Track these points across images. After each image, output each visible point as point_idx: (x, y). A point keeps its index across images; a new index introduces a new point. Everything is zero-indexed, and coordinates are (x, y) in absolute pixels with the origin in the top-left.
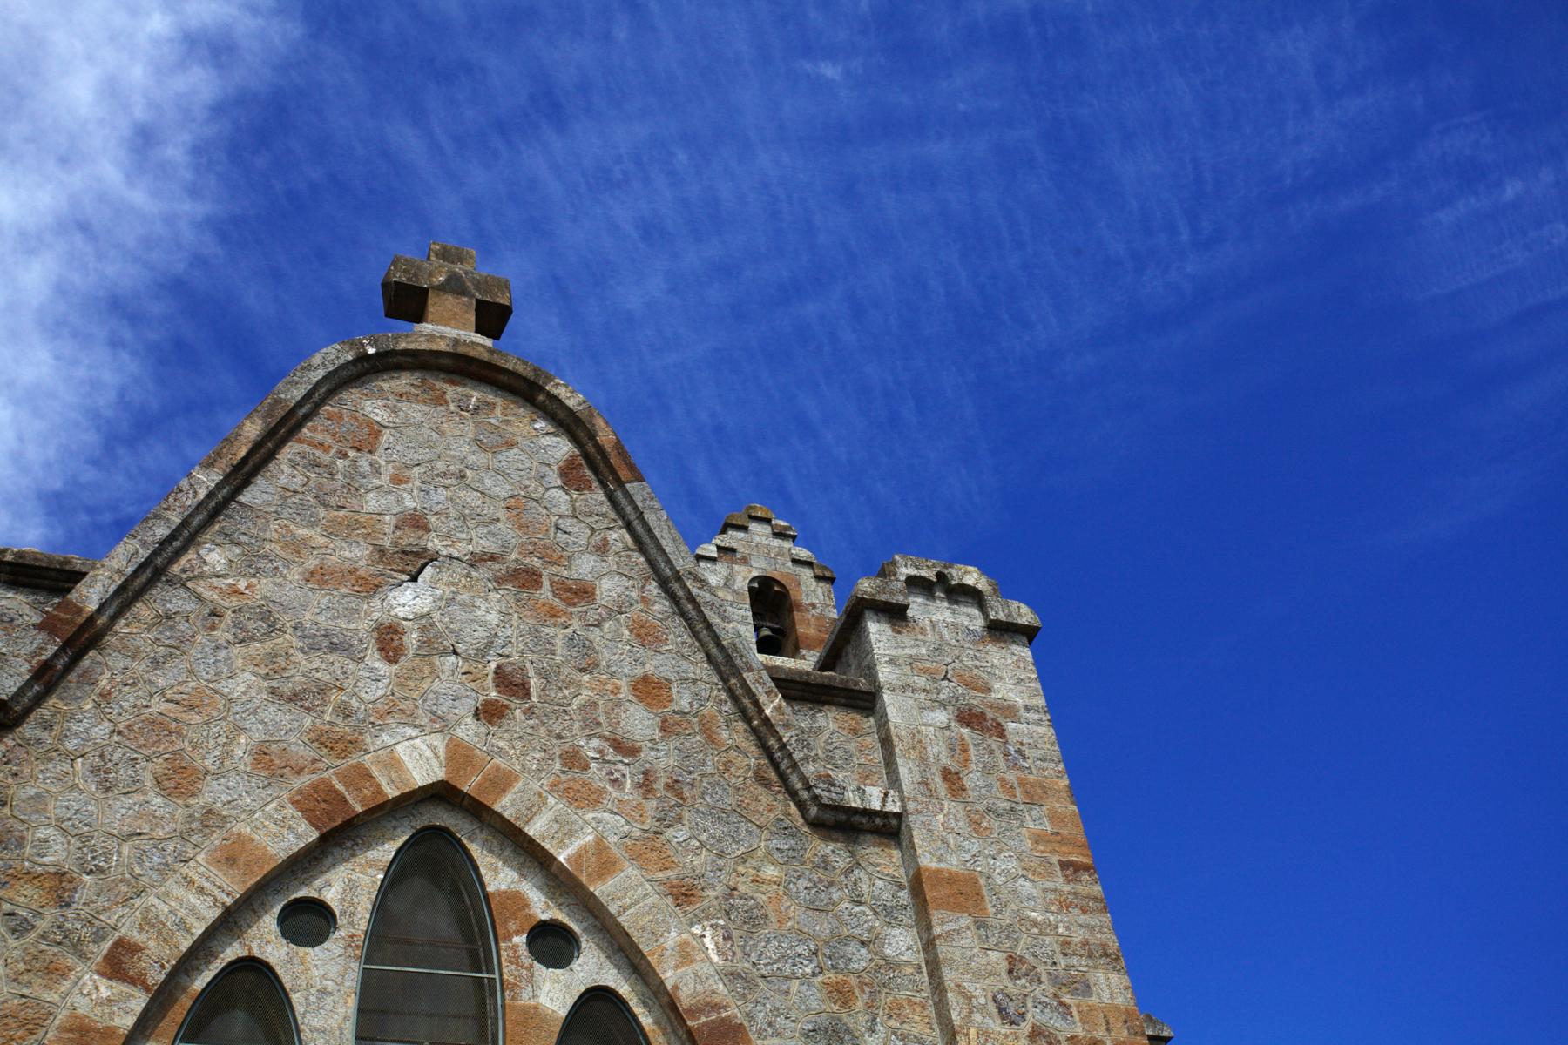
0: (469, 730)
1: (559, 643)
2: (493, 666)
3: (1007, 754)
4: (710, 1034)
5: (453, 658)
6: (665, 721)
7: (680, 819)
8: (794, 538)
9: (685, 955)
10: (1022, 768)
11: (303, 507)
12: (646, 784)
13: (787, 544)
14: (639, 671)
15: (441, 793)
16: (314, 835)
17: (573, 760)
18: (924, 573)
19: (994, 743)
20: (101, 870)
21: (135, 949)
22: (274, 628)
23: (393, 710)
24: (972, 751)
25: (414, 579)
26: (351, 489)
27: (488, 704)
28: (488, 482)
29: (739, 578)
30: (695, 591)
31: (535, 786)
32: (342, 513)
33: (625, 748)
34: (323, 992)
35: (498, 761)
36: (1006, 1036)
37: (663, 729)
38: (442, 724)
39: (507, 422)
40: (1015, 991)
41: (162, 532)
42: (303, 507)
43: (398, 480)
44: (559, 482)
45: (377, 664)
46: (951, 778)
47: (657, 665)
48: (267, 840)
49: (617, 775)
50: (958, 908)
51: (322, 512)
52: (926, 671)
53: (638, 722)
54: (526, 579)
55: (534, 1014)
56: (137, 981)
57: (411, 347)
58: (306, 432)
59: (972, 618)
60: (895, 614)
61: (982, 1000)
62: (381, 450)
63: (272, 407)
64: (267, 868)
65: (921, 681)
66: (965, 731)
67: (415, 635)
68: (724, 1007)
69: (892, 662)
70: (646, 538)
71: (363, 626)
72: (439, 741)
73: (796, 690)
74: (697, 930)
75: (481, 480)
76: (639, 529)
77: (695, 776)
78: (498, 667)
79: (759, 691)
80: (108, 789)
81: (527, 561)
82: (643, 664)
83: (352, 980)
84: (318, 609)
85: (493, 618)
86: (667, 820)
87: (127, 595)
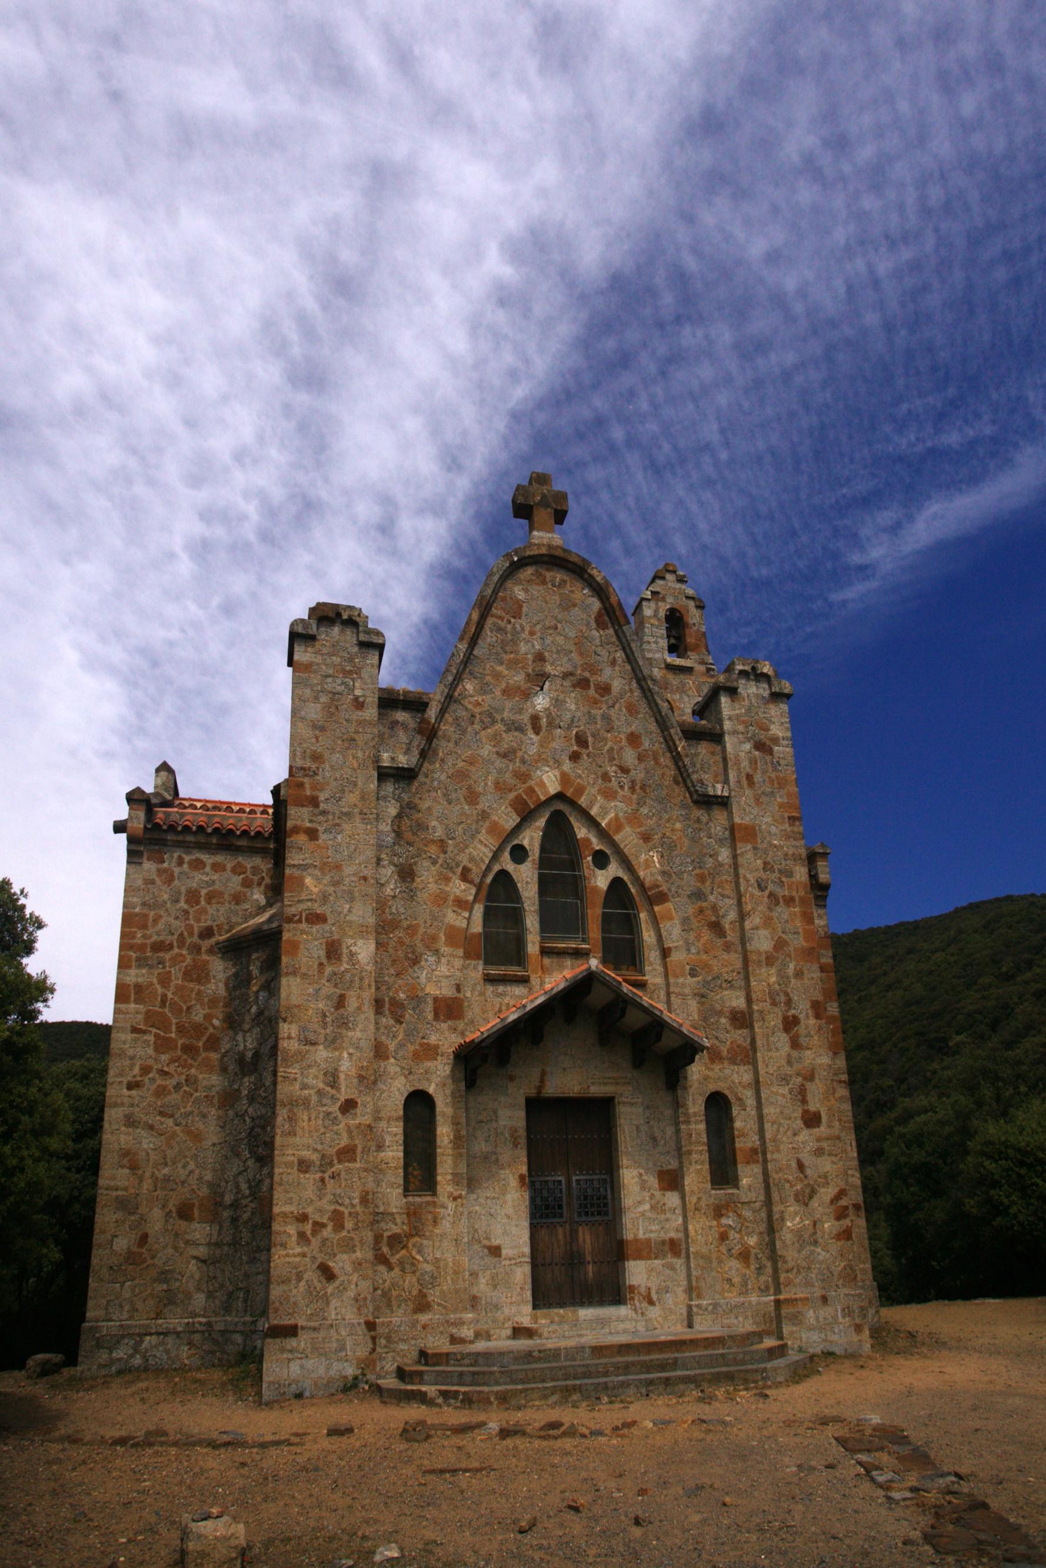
0: (567, 766)
1: (599, 718)
3: (773, 764)
12: (632, 789)
14: (629, 731)
15: (560, 796)
16: (518, 820)
17: (606, 777)
19: (768, 758)
22: (494, 722)
25: (542, 689)
32: (512, 656)
33: (625, 770)
34: (527, 883)
35: (579, 780)
38: (558, 763)
39: (572, 592)
43: (532, 633)
45: (532, 736)
46: (749, 777)
47: (635, 726)
50: (747, 841)
52: (743, 722)
53: (629, 756)
54: (583, 684)
55: (596, 889)
56: (471, 882)
62: (523, 617)
65: (741, 728)
71: (525, 718)
72: (557, 773)
79: (676, 738)
84: (508, 709)
85: (573, 707)
86: (641, 803)
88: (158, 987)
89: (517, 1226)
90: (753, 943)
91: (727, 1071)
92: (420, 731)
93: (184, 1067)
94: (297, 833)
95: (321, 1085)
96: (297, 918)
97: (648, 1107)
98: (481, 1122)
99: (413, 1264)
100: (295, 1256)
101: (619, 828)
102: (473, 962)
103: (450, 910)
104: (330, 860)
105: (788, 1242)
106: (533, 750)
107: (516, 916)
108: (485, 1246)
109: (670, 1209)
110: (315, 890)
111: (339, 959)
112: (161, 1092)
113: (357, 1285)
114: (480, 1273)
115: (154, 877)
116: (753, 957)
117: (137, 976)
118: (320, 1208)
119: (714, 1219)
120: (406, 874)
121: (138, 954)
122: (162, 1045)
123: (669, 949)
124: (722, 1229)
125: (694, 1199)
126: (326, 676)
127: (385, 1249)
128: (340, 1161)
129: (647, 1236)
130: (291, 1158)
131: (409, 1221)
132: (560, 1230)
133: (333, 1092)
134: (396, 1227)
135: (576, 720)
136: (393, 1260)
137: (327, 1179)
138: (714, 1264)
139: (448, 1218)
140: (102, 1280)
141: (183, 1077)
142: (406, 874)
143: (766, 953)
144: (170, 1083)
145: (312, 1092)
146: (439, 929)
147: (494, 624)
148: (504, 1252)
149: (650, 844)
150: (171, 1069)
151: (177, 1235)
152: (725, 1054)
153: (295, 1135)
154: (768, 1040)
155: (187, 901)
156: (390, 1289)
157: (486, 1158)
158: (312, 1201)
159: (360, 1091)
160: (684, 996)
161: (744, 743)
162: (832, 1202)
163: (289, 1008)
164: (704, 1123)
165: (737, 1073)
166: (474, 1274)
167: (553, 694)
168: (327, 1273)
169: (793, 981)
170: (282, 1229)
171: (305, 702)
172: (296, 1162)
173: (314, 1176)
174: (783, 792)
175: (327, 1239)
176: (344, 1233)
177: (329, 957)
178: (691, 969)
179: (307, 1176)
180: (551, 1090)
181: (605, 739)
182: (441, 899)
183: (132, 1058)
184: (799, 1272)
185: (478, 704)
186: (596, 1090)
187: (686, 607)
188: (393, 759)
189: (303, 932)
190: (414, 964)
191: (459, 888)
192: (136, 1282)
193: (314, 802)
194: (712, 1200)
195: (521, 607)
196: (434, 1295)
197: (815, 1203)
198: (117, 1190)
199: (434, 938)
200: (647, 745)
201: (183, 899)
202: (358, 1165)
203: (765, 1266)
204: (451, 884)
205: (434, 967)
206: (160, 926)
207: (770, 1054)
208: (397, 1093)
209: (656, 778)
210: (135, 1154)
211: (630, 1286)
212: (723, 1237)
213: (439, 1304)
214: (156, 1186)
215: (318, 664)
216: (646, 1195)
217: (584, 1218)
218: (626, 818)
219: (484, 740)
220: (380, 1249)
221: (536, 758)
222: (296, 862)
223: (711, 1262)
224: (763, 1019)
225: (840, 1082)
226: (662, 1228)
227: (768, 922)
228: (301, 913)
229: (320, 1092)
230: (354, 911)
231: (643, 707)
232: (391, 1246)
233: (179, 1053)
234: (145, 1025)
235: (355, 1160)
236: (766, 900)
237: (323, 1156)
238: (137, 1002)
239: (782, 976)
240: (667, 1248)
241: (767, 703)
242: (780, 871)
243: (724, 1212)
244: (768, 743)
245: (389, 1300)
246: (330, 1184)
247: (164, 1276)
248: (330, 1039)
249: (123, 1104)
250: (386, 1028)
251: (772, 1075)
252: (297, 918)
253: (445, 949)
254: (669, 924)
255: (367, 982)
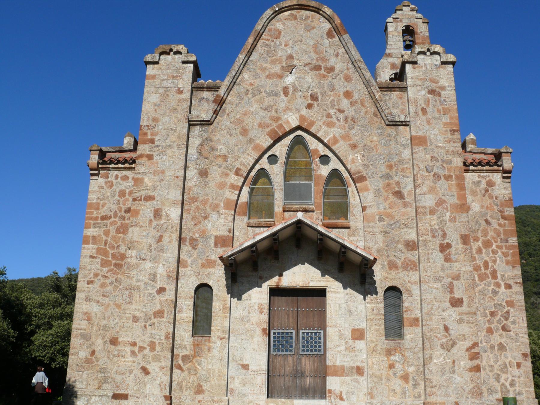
1: (326, 85)
2: (310, 94)
3: (440, 101)
6: (351, 102)
7: (354, 128)
9: (353, 161)
10: (444, 105)
11: (264, 58)
12: (346, 120)
14: (345, 90)
15: (299, 128)
16: (272, 142)
17: (329, 116)
19: (437, 98)
22: (260, 92)
23: (287, 109)
25: (291, 73)
28: (308, 41)
29: (399, 27)
30: (360, 65)
32: (274, 58)
33: (341, 111)
34: (277, 174)
38: (298, 110)
39: (313, 21)
41: (234, 73)
42: (264, 58)
43: (286, 45)
46: (424, 111)
48: (263, 144)
51: (269, 59)
52: (421, 79)
53: (345, 103)
54: (318, 68)
55: (320, 176)
56: (241, 176)
58: (263, 36)
62: (281, 37)
65: (419, 83)
66: (430, 96)
70: (348, 50)
71: (280, 89)
72: (298, 116)
73: (384, 88)
74: (356, 155)
75: (306, 41)
76: (346, 48)
79: (375, 91)
83: (282, 171)
84: (269, 85)
85: (310, 80)
86: (351, 128)
87: (229, 90)
88: (103, 236)
89: (259, 354)
91: (401, 275)
92: (215, 101)
93: (114, 274)
94: (142, 157)
95: (147, 280)
96: (138, 199)
99: (195, 370)
101: (336, 141)
102: (241, 217)
103: (227, 190)
105: (434, 371)
106: (283, 105)
111: (160, 217)
112: (103, 285)
113: (161, 378)
115: (104, 185)
116: (420, 210)
117: (93, 232)
118: (144, 340)
122: (104, 264)
126: (163, 80)
129: (341, 364)
130: (129, 315)
132: (290, 358)
133: (153, 283)
135: (311, 87)
136: (184, 368)
137: (148, 326)
138: (384, 381)
139: (217, 349)
140: (73, 370)
141: (114, 279)
144: (108, 281)
145: (142, 283)
146: (221, 200)
147: (263, 43)
148: (250, 368)
149: (355, 150)
150: (109, 275)
151: (109, 352)
152: (400, 265)
153: (132, 304)
154: (428, 257)
155: (119, 196)
157: (243, 319)
158: (139, 336)
159: (168, 283)
161: (421, 90)
162: (467, 350)
164: (383, 303)
165: (408, 276)
168: (146, 371)
169: (448, 223)
174: (447, 116)
176: (156, 352)
177: (155, 217)
178: (379, 218)
179: (137, 324)
181: (329, 96)
182: (222, 186)
183: (90, 270)
184: (440, 388)
185: (251, 84)
187: (416, 24)
189: (142, 205)
190: (205, 219)
192: (90, 371)
193: (152, 141)
196: (206, 386)
197: (455, 350)
198: (81, 330)
200: (357, 97)
201: (117, 195)
202: (164, 320)
203: (419, 384)
204: (229, 177)
206: (105, 208)
207: (429, 265)
209: (362, 114)
210: (90, 314)
211: (329, 390)
212: (391, 366)
213: (209, 391)
214: (99, 329)
215: (159, 75)
216: (343, 342)
222: (140, 171)
223: (381, 380)
224: (425, 245)
225: (516, 283)
227: (432, 190)
229: (146, 283)
232: (183, 361)
233: (112, 267)
234: (96, 254)
235: (163, 317)
236: (432, 177)
237: (146, 315)
238: (93, 244)
239: (441, 221)
240: (355, 371)
241: (439, 67)
242: (443, 161)
243: (393, 352)
247: (103, 370)
248: (153, 257)
249: (85, 291)
252: (138, 199)
253: (222, 211)
254: (366, 193)
255: (175, 228)
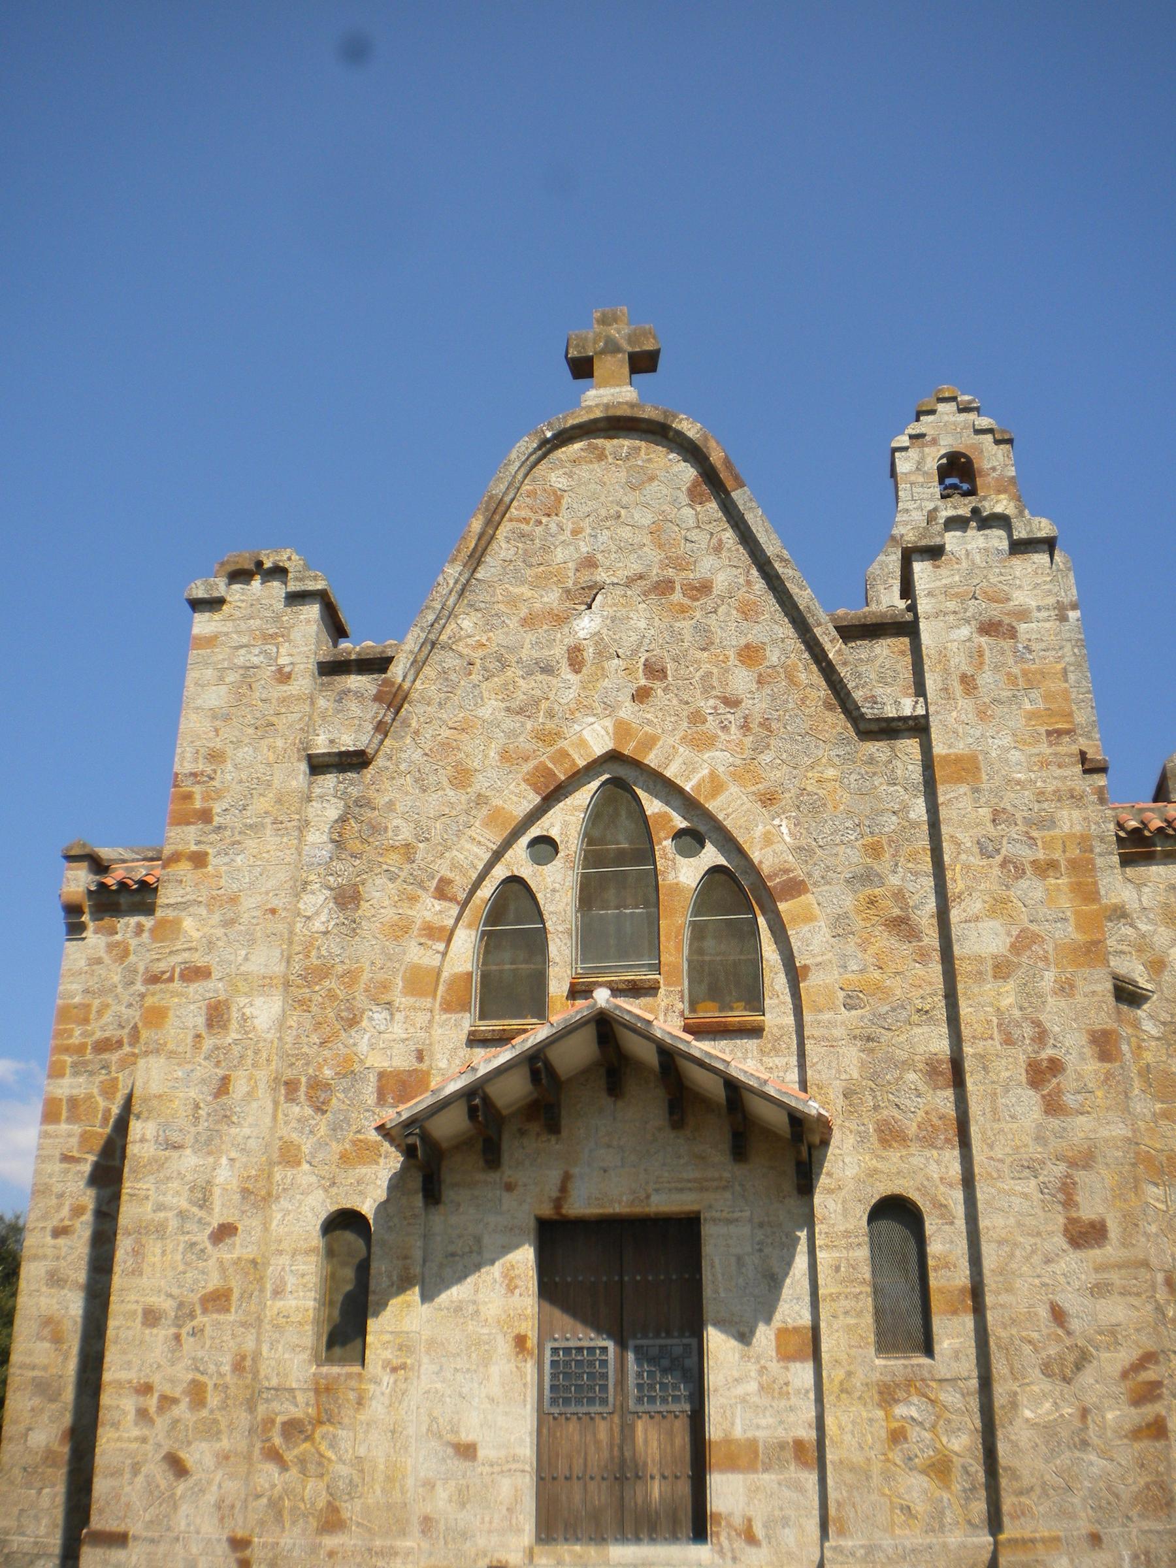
0: (628, 711)
2: (643, 660)
4: (782, 889)
5: (616, 661)
7: (768, 746)
8: (977, 409)
12: (745, 727)
13: (972, 416)
14: (743, 642)
15: (614, 757)
16: (538, 799)
17: (697, 718)
18: (960, 512)
19: (1007, 644)
20: (427, 839)
21: (449, 882)
22: (504, 666)
23: (582, 707)
24: (987, 653)
25: (590, 607)
26: (545, 549)
27: (639, 689)
28: (637, 516)
29: (929, 459)
31: (671, 741)
32: (542, 568)
33: (732, 702)
34: (554, 890)
35: (647, 728)
36: (983, 867)
37: (759, 682)
38: (610, 708)
39: (649, 460)
40: (995, 834)
41: (431, 617)
43: (575, 532)
44: (687, 501)
45: (569, 677)
46: (967, 681)
47: (756, 633)
49: (726, 722)
50: (960, 780)
51: (529, 572)
52: (957, 595)
53: (741, 680)
55: (676, 888)
56: (452, 899)
57: (576, 421)
59: (997, 539)
60: (935, 553)
61: (969, 844)
63: (488, 503)
64: (513, 824)
65: (951, 605)
67: (591, 650)
68: (792, 871)
69: (930, 594)
71: (558, 652)
72: (609, 723)
74: (777, 822)
77: (781, 712)
78: (646, 660)
80: (425, 791)
81: (665, 573)
82: (746, 635)
84: (529, 646)
85: (642, 624)
86: (760, 747)
88: (99, 1099)
89: (506, 1414)
90: (967, 944)
95: (184, 1205)
97: (761, 1225)
98: (453, 1255)
99: (320, 1464)
100: (130, 1440)
102: (454, 1016)
103: (413, 943)
104: (222, 891)
105: (1024, 1443)
107: (537, 943)
108: (449, 1444)
109: (798, 1391)
110: (196, 935)
111: (225, 1027)
114: (439, 1483)
117: (71, 1087)
118: (173, 1376)
119: (879, 1405)
120: (347, 898)
121: (75, 1058)
123: (806, 967)
124: (895, 1425)
125: (840, 1374)
127: (277, 1440)
128: (205, 1311)
129: (750, 1435)
130: (134, 1307)
131: (317, 1401)
134: (300, 1407)
136: (289, 1456)
137: (184, 1336)
138: (876, 1480)
142: (347, 898)
143: (994, 957)
145: (170, 1214)
146: (395, 971)
148: (481, 1453)
152: (912, 1129)
153: (141, 1274)
154: (993, 1101)
156: (281, 1498)
158: (159, 1366)
159: (243, 1212)
160: (831, 1043)
162: (1125, 1375)
163: (145, 1100)
165: (938, 1162)
166: (430, 1485)
167: (610, 611)
170: (114, 1403)
171: (203, 686)
172: (140, 1311)
173: (163, 1333)
174: (1035, 694)
175: (178, 1421)
176: (204, 1413)
177: (210, 1025)
179: (155, 1331)
180: (580, 1205)
182: (401, 929)
183: (61, 1196)
186: (663, 1203)
188: (332, 742)
189: (175, 994)
190: (351, 1026)
191: (431, 909)
193: (205, 816)
194: (876, 1376)
195: (559, 499)
196: (350, 1510)
197: (1087, 1377)
199: (385, 986)
202: (231, 1317)
205: (382, 1028)
206: (107, 1018)
208: (310, 1215)
213: (358, 1524)
215: (227, 634)
216: (753, 1368)
217: (646, 1407)
218: (733, 774)
219: (486, 694)
220: (269, 1440)
221: (573, 706)
222: (172, 901)
224: (985, 1068)
226: (781, 1422)
228: (173, 969)
229: (182, 1215)
230: (252, 958)
231: (771, 604)
236: (996, 871)
237: (181, 1305)
238: (69, 1120)
239: (1030, 995)
240: (789, 1454)
244: (1007, 620)
245: (280, 1513)
246: (188, 1343)
249: (45, 1257)
250: (299, 1121)
251: (1002, 1161)
254: (806, 928)
255: (265, 1055)
